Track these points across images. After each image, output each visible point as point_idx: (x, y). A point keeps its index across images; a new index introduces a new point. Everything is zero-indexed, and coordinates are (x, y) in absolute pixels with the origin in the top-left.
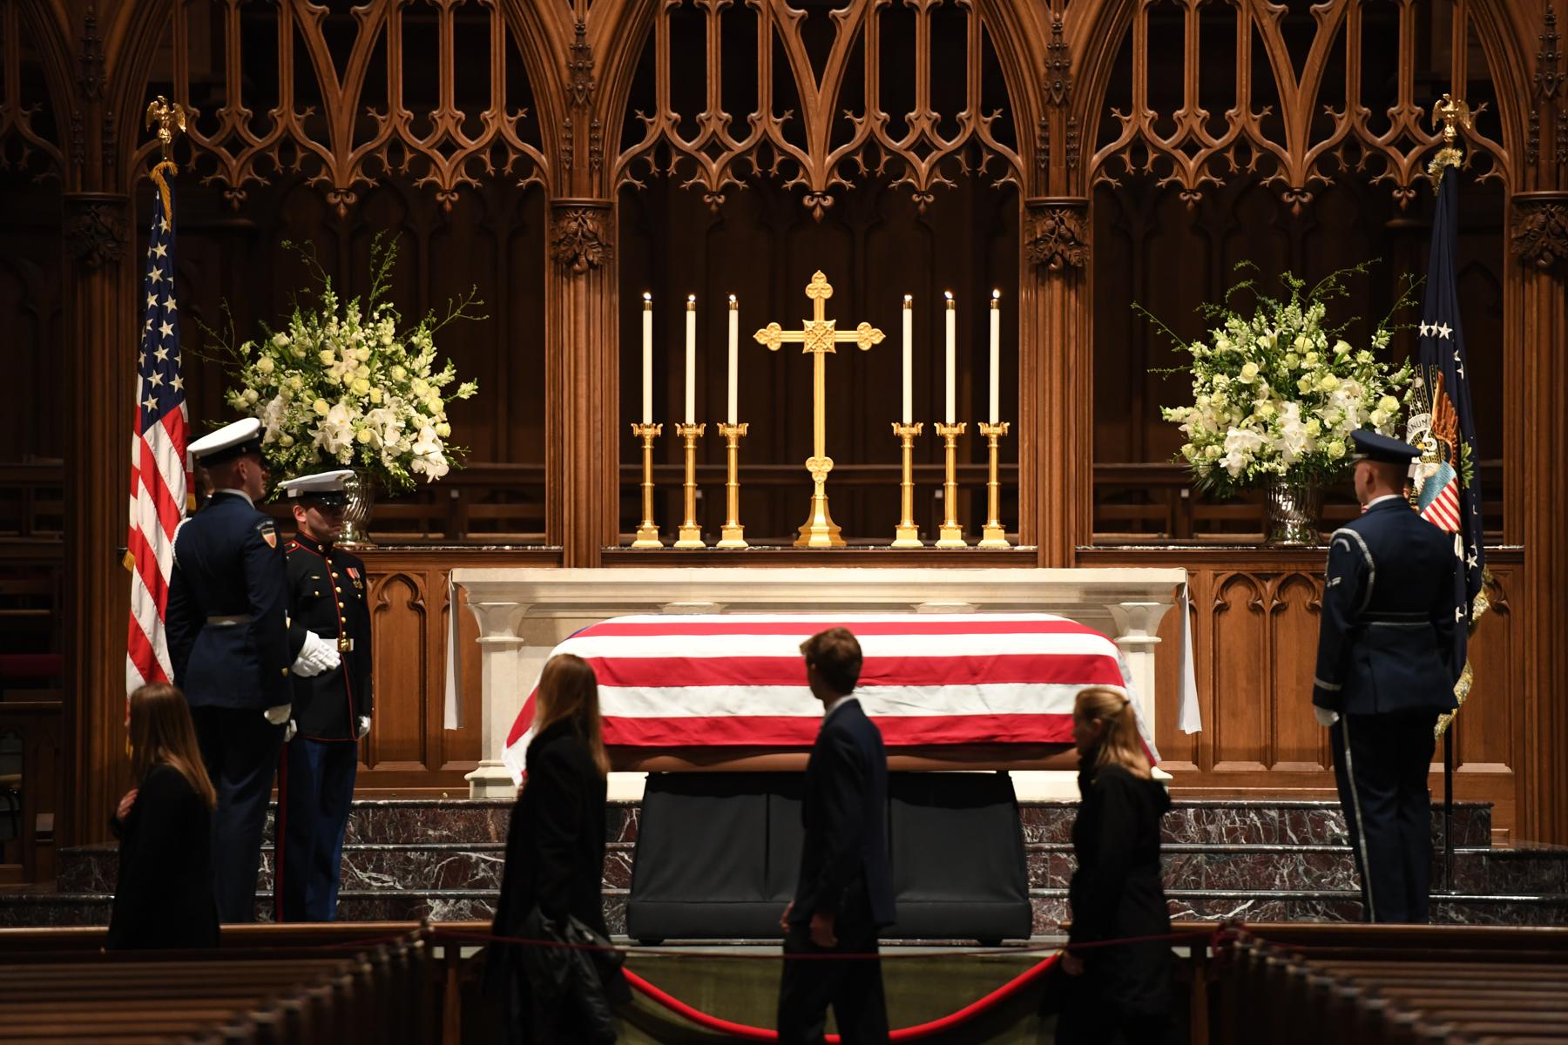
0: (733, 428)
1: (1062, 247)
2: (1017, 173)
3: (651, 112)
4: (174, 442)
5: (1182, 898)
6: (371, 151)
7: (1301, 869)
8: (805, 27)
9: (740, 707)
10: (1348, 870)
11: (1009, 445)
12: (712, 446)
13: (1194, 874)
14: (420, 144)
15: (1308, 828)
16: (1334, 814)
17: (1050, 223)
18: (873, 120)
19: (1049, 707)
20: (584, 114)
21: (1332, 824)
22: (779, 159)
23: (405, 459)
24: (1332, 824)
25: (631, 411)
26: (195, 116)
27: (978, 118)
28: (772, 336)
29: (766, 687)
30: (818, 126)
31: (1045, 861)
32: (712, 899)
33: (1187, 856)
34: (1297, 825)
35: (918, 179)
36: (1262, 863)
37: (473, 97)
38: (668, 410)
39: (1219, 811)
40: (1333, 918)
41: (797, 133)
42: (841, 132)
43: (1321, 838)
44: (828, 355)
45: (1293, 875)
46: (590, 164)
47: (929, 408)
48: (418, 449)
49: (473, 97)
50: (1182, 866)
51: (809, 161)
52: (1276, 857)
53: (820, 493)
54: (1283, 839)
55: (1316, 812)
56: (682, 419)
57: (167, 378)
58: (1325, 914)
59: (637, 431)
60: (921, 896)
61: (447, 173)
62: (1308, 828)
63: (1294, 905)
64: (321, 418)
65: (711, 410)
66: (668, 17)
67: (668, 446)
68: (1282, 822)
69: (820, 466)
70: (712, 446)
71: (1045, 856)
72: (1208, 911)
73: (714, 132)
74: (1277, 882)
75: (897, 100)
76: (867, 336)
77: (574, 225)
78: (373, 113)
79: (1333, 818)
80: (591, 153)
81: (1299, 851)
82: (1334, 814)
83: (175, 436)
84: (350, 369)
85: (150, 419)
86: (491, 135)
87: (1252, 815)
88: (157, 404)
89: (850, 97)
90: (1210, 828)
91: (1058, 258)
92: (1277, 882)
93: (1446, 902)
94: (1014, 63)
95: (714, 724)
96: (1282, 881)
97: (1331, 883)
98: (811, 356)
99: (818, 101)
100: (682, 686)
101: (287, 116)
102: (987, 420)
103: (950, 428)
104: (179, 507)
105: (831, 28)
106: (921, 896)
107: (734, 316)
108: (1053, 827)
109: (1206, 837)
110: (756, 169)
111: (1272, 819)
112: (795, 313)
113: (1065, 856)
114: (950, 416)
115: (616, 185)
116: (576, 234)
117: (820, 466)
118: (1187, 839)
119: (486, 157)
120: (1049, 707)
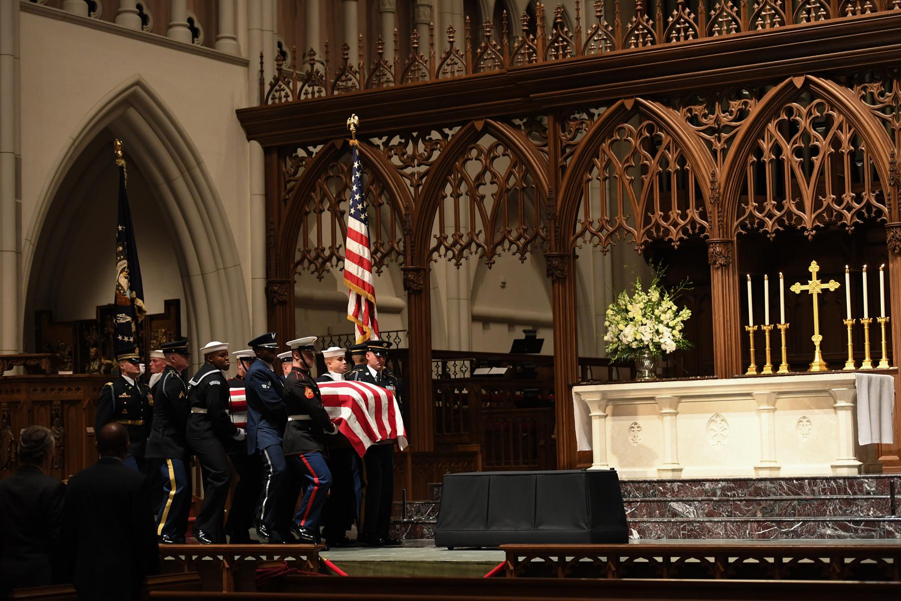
0: (783, 326)
1: (898, 243)
2: (885, 216)
3: (824, 197)
5: (772, 522)
6: (649, 229)
7: (838, 507)
8: (802, 165)
10: (858, 507)
11: (888, 325)
12: (775, 333)
13: (793, 510)
14: (759, 215)
15: (856, 487)
16: (867, 481)
17: (892, 233)
18: (829, 198)
20: (715, 206)
21: (866, 485)
22: (794, 218)
23: (658, 346)
24: (866, 485)
25: (745, 321)
26: (661, 215)
27: (869, 195)
28: (797, 288)
30: (808, 203)
31: (731, 505)
33: (790, 502)
34: (851, 486)
35: (847, 221)
36: (821, 504)
37: (684, 205)
38: (759, 320)
39: (818, 481)
40: (836, 530)
41: (800, 207)
42: (817, 204)
43: (861, 491)
44: (818, 294)
45: (835, 509)
46: (719, 226)
47: (857, 313)
48: (662, 341)
49: (684, 205)
50: (788, 507)
51: (805, 217)
52: (827, 501)
53: (818, 349)
54: (846, 493)
55: (859, 480)
56: (863, 317)
58: (832, 528)
59: (862, 322)
61: (675, 234)
62: (856, 487)
63: (819, 524)
64: (622, 331)
65: (775, 319)
66: (752, 167)
67: (759, 334)
68: (845, 485)
69: (817, 339)
70: (775, 333)
71: (731, 503)
72: (783, 527)
73: (769, 210)
74: (828, 513)
75: (839, 190)
76: (833, 285)
77: (712, 249)
78: (649, 214)
79: (866, 483)
80: (719, 221)
81: (836, 499)
82: (867, 481)
84: (635, 311)
86: (865, 202)
87: (832, 482)
89: (820, 190)
90: (815, 488)
91: (897, 248)
92: (828, 513)
93: (884, 521)
94: (881, 171)
96: (830, 512)
97: (851, 513)
98: (812, 295)
99: (808, 193)
101: (790, 204)
102: (780, 323)
103: (866, 320)
105: (812, 165)
107: (782, 281)
108: (750, 490)
109: (813, 492)
110: (787, 222)
111: (841, 484)
112: (805, 278)
113: (739, 503)
114: (767, 322)
115: (735, 232)
116: (713, 253)
117: (817, 339)
118: (805, 493)
119: (689, 227)
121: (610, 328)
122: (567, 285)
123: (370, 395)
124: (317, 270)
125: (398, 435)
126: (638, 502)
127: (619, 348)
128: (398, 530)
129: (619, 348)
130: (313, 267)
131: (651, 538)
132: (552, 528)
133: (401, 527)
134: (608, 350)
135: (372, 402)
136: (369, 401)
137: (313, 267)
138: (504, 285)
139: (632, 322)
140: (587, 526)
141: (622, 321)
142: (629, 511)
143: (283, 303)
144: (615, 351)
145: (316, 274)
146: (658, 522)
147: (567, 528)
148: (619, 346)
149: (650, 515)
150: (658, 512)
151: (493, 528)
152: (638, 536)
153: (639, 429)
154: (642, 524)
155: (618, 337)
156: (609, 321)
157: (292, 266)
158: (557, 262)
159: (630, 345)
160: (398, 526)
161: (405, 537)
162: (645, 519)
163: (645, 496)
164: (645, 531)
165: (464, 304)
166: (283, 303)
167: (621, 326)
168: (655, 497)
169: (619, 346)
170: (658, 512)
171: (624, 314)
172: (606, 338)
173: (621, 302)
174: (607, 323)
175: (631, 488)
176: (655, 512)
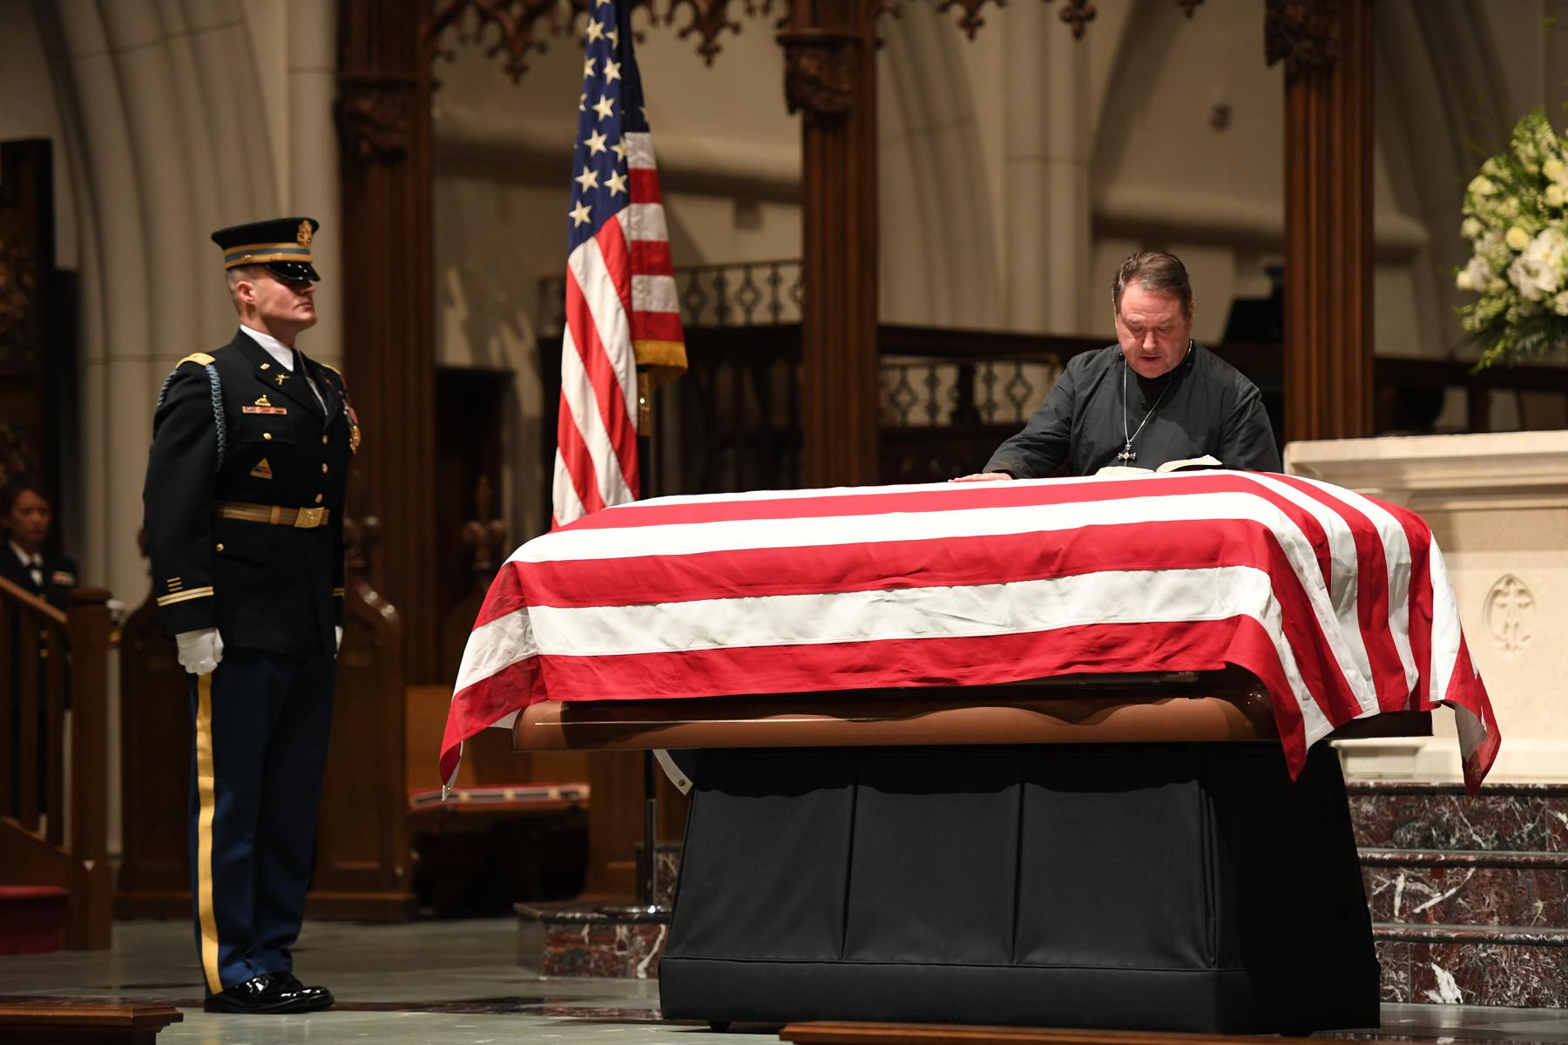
4: (609, 267)
9: (729, 633)
19: (1162, 607)
29: (765, 599)
32: (771, 956)
57: (603, 177)
60: (1057, 958)
64: (1517, 253)
83: (610, 258)
85: (583, 234)
88: (590, 215)
95: (692, 662)
100: (653, 603)
104: (613, 360)
106: (1057, 958)
120: (1162, 607)
121: (1478, 246)
122: (1338, 90)
123: (1335, 526)
124: (505, 43)
125: (529, 608)
126: (1466, 865)
127: (1511, 315)
128: (622, 946)
129: (1511, 315)
130: (492, 33)
131: (1504, 1003)
132: (1080, 959)
133: (632, 936)
134: (1471, 324)
135: (1345, 552)
136: (1335, 552)
137: (492, 33)
138: (1222, 117)
139: (1556, 223)
140: (1202, 956)
141: (1522, 220)
142: (1437, 898)
143: (393, 157)
144: (1496, 325)
145: (503, 57)
146: (1529, 942)
147: (1131, 964)
148: (1507, 307)
149: (1513, 915)
150: (1540, 904)
151: (868, 955)
152: (1458, 993)
153: (1524, 600)
154: (1469, 950)
155: (1503, 275)
156: (1479, 219)
157: (423, 29)
158: (1301, 10)
159: (1549, 303)
160: (622, 931)
161: (647, 970)
162: (1494, 929)
163: (1503, 846)
164: (1481, 977)
165: (1064, 180)
166: (393, 157)
167: (1517, 236)
168: (1542, 847)
169: (1507, 307)
170: (1540, 904)
171: (1531, 194)
172: (1465, 279)
173: (1526, 151)
174: (1471, 227)
175: (1455, 812)
176: (1529, 904)
